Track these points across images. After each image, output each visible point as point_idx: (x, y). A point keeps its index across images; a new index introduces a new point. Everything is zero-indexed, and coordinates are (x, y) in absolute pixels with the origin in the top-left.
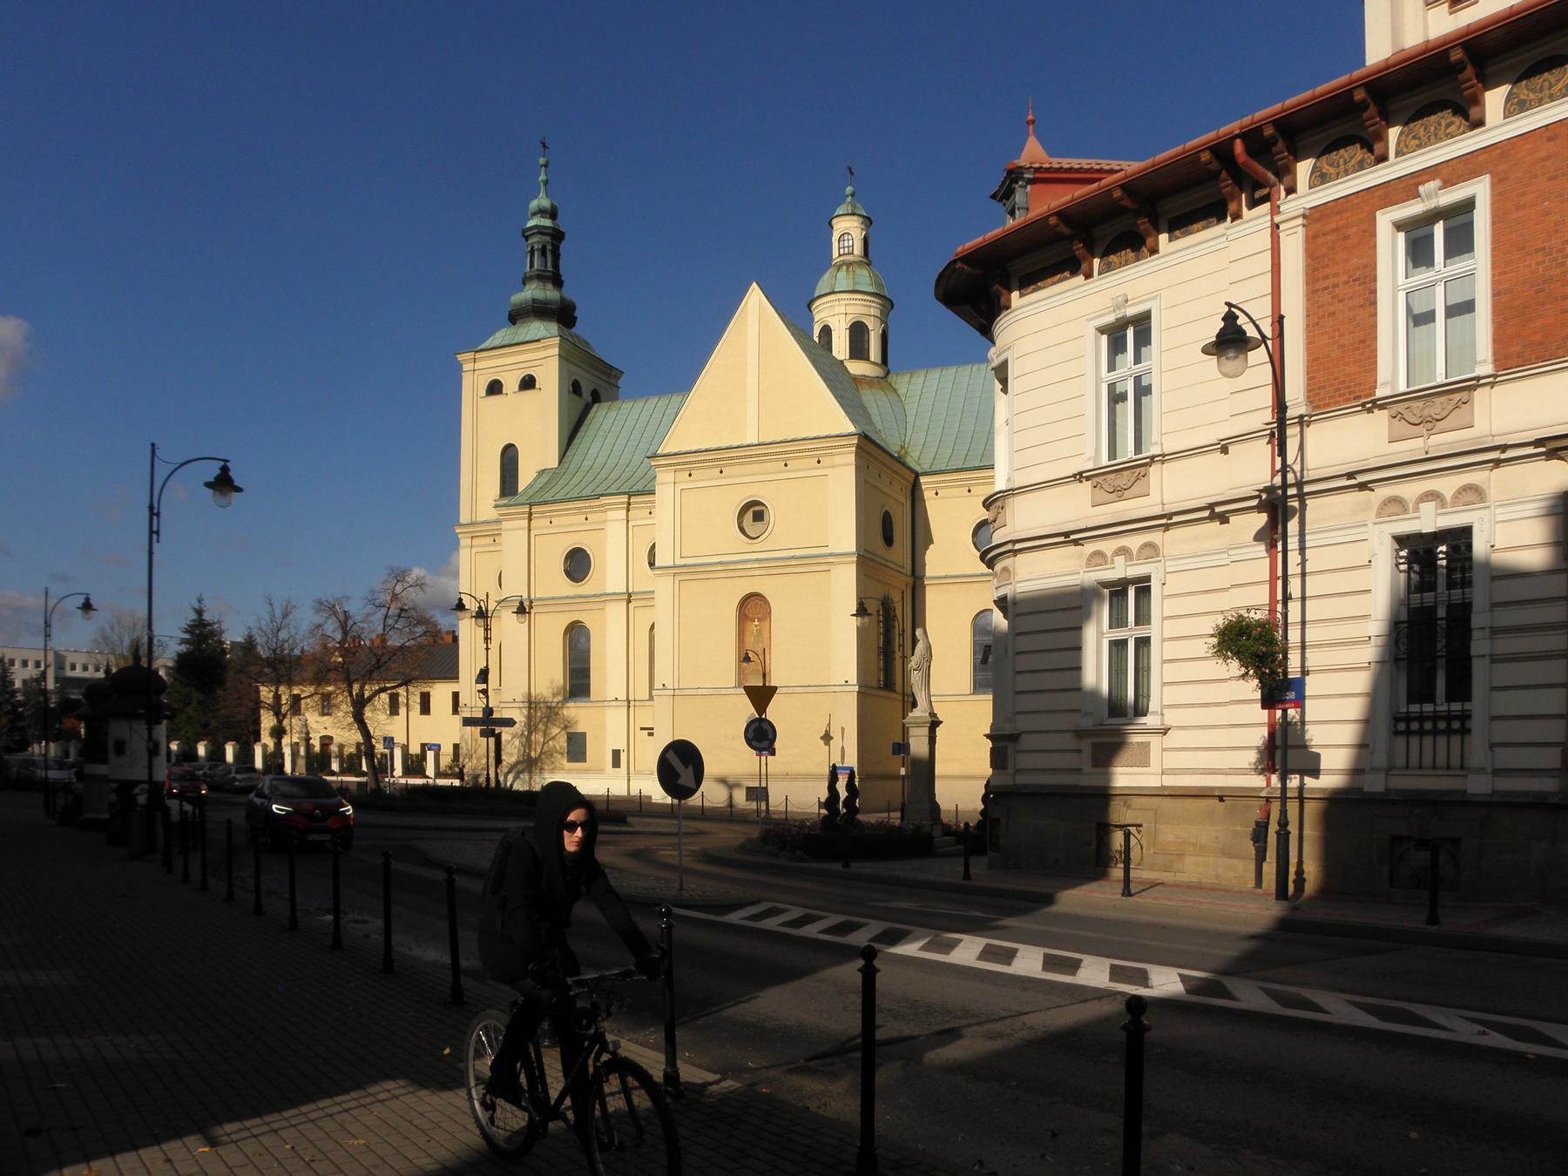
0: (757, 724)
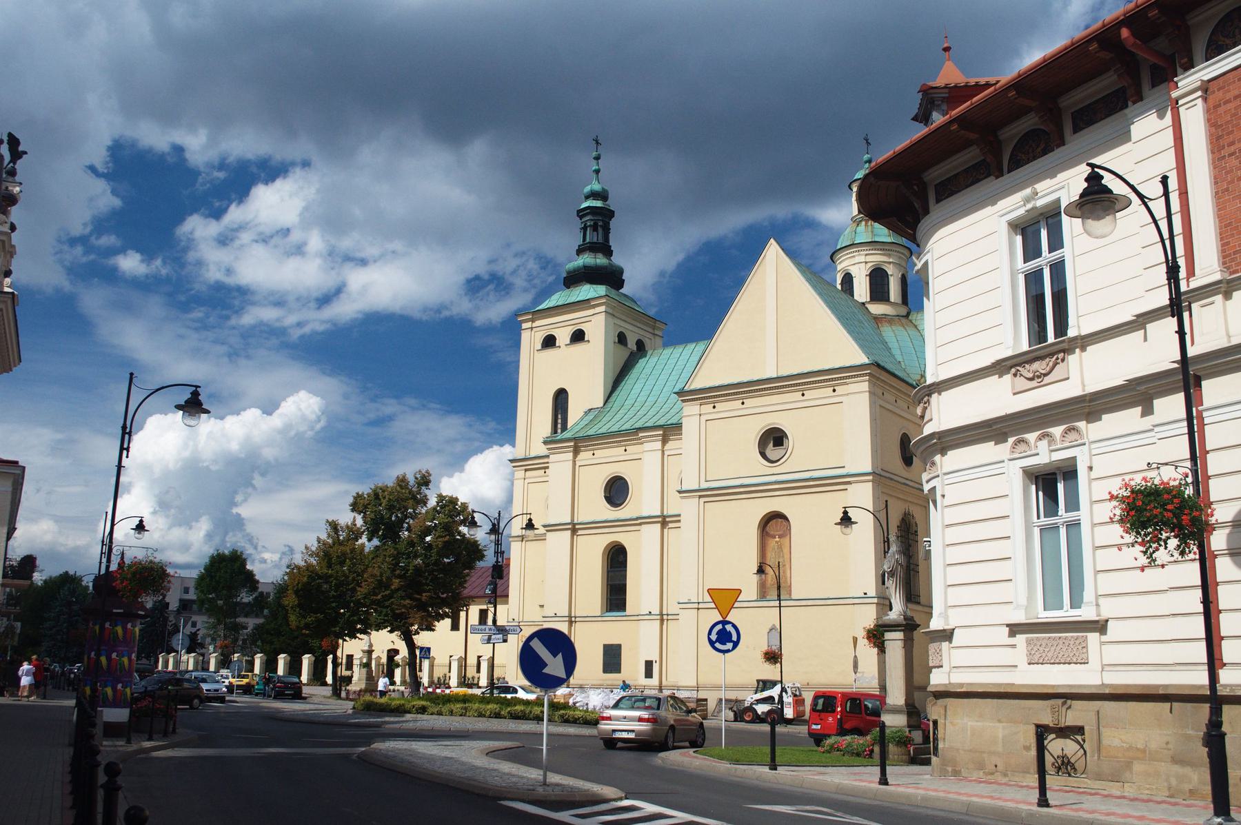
0: (720, 627)
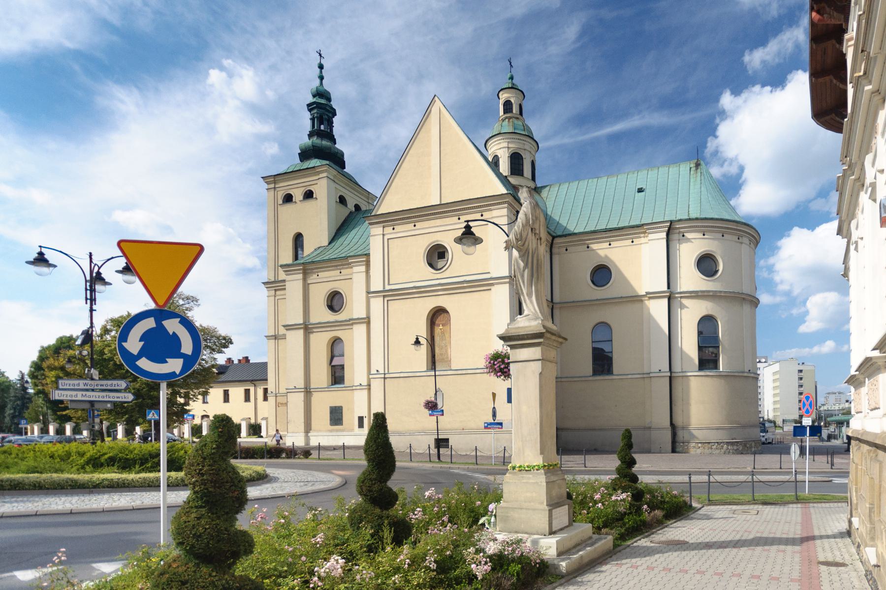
0: (149, 323)
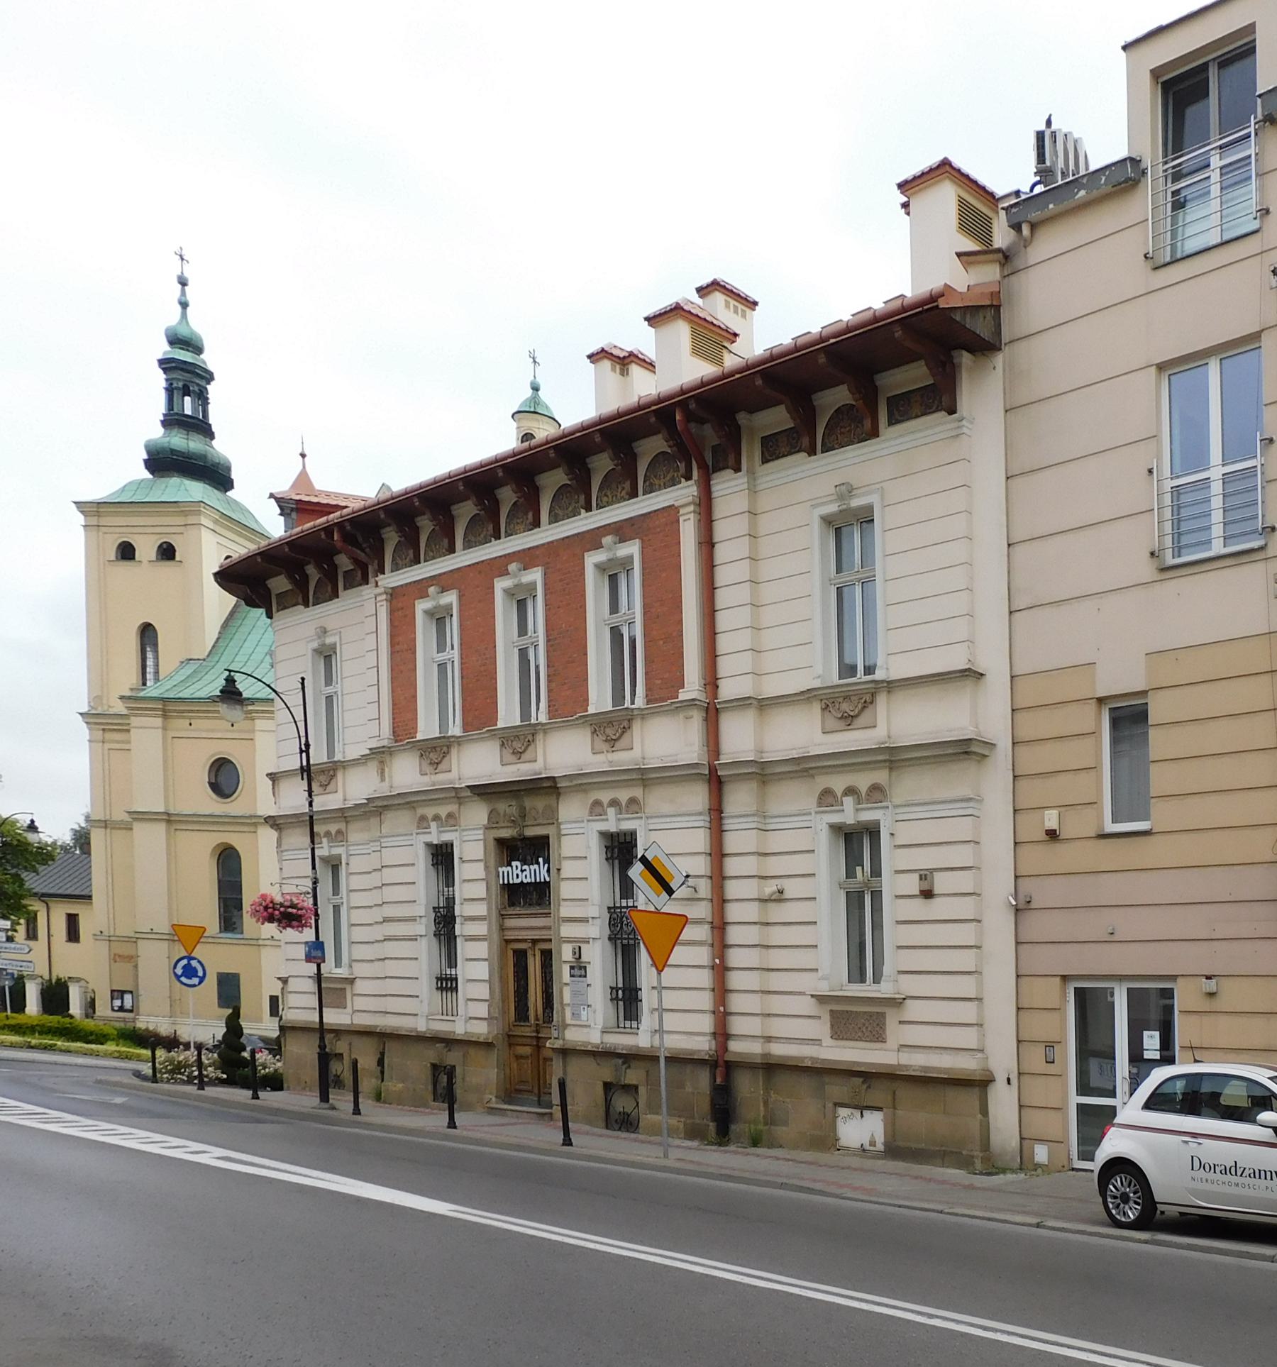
0: (185, 962)
